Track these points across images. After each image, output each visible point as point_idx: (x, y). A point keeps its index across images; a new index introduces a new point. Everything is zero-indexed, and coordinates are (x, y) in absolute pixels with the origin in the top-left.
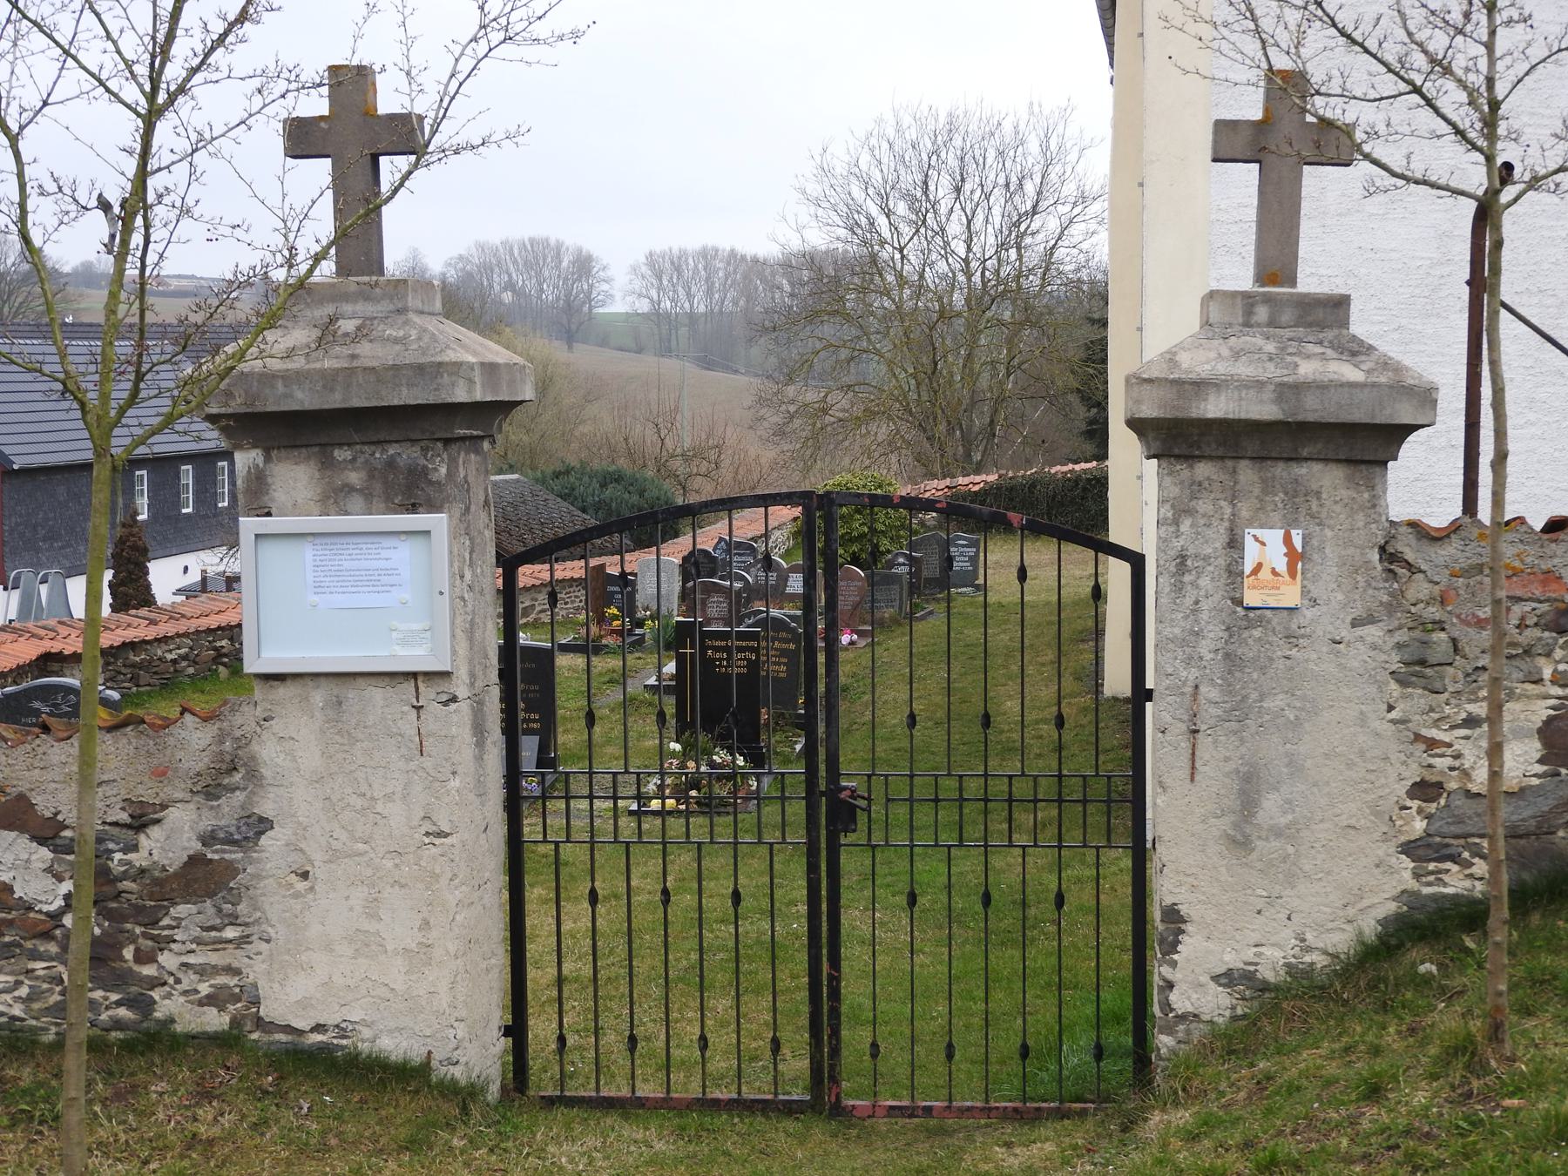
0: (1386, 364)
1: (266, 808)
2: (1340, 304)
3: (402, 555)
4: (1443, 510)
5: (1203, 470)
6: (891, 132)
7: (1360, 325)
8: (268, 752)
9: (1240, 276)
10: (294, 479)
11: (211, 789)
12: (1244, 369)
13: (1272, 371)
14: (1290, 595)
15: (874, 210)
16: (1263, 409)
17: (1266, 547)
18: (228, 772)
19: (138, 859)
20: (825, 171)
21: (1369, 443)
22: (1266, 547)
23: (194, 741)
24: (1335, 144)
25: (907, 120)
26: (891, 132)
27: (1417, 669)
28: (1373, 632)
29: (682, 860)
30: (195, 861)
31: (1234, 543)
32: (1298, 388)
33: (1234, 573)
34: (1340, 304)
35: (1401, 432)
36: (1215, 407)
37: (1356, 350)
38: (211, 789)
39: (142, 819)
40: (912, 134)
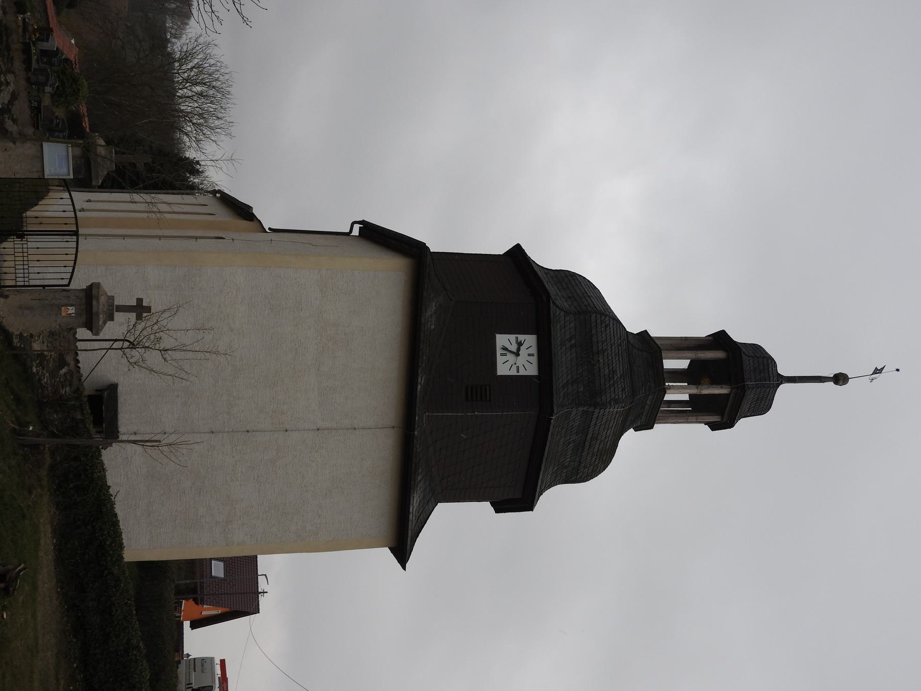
0: (102, 328)
1: (18, 144)
2: (112, 319)
3: (65, 170)
4: (78, 336)
5: (84, 300)
6: (222, 71)
7: (109, 323)
8: (28, 145)
9: (117, 302)
10: (78, 151)
11: (21, 133)
12: (101, 306)
13: (101, 311)
14: (63, 314)
15: (196, 61)
16: (94, 310)
17: (71, 310)
18: (23, 137)
19: (6, 120)
20: (208, 45)
21: (90, 325)
22: (71, 310)
23: (30, 131)
24: (139, 318)
25: (227, 77)
26: (222, 71)
27: (52, 334)
28: (58, 327)
29: (31, 270)
30: (7, 130)
31: (72, 305)
32: (98, 315)
33: (67, 305)
34: (112, 319)
35: (91, 329)
36: (94, 303)
37: (105, 323)
38: (21, 133)
39: (15, 121)
40: (221, 78)
